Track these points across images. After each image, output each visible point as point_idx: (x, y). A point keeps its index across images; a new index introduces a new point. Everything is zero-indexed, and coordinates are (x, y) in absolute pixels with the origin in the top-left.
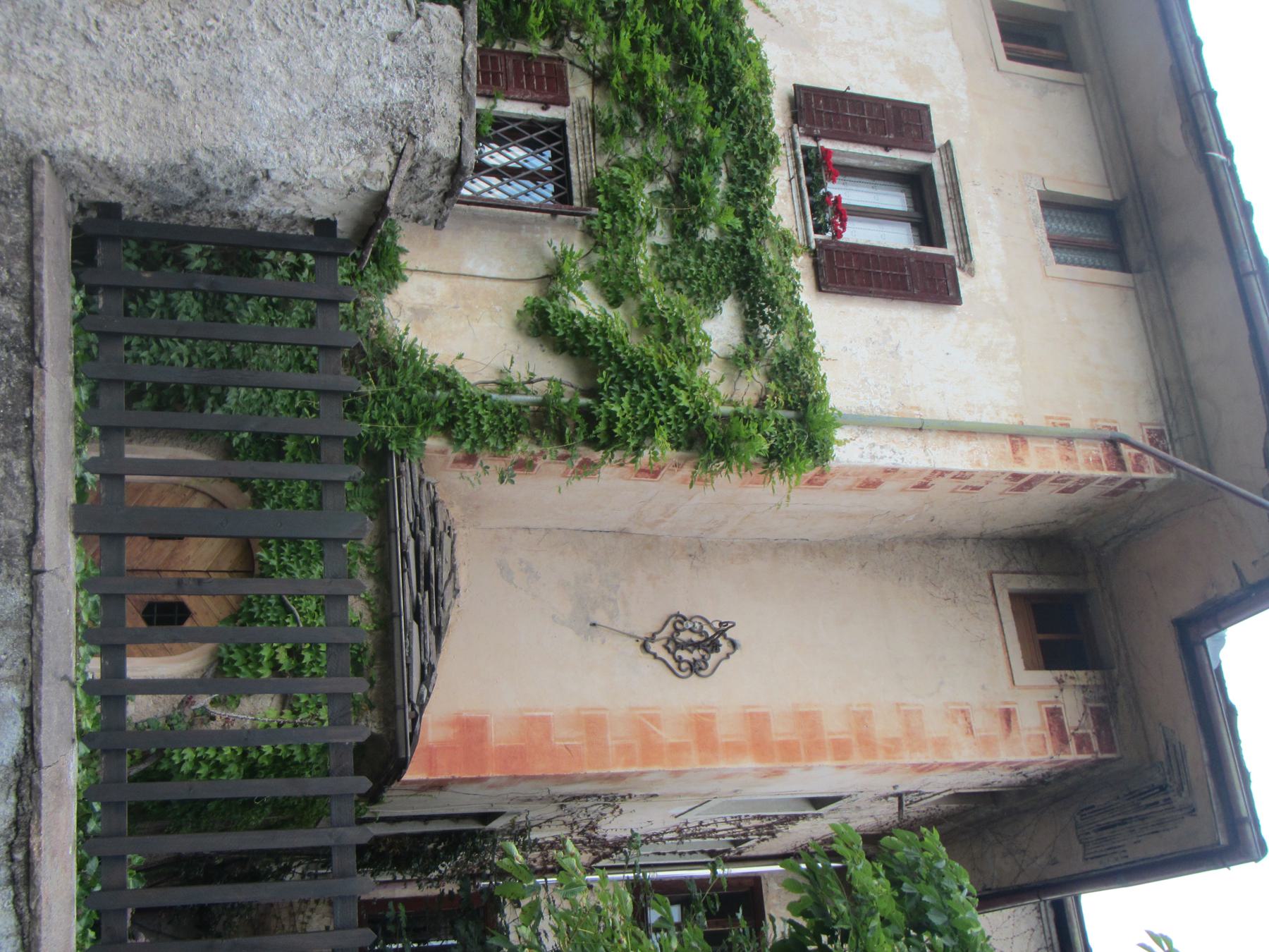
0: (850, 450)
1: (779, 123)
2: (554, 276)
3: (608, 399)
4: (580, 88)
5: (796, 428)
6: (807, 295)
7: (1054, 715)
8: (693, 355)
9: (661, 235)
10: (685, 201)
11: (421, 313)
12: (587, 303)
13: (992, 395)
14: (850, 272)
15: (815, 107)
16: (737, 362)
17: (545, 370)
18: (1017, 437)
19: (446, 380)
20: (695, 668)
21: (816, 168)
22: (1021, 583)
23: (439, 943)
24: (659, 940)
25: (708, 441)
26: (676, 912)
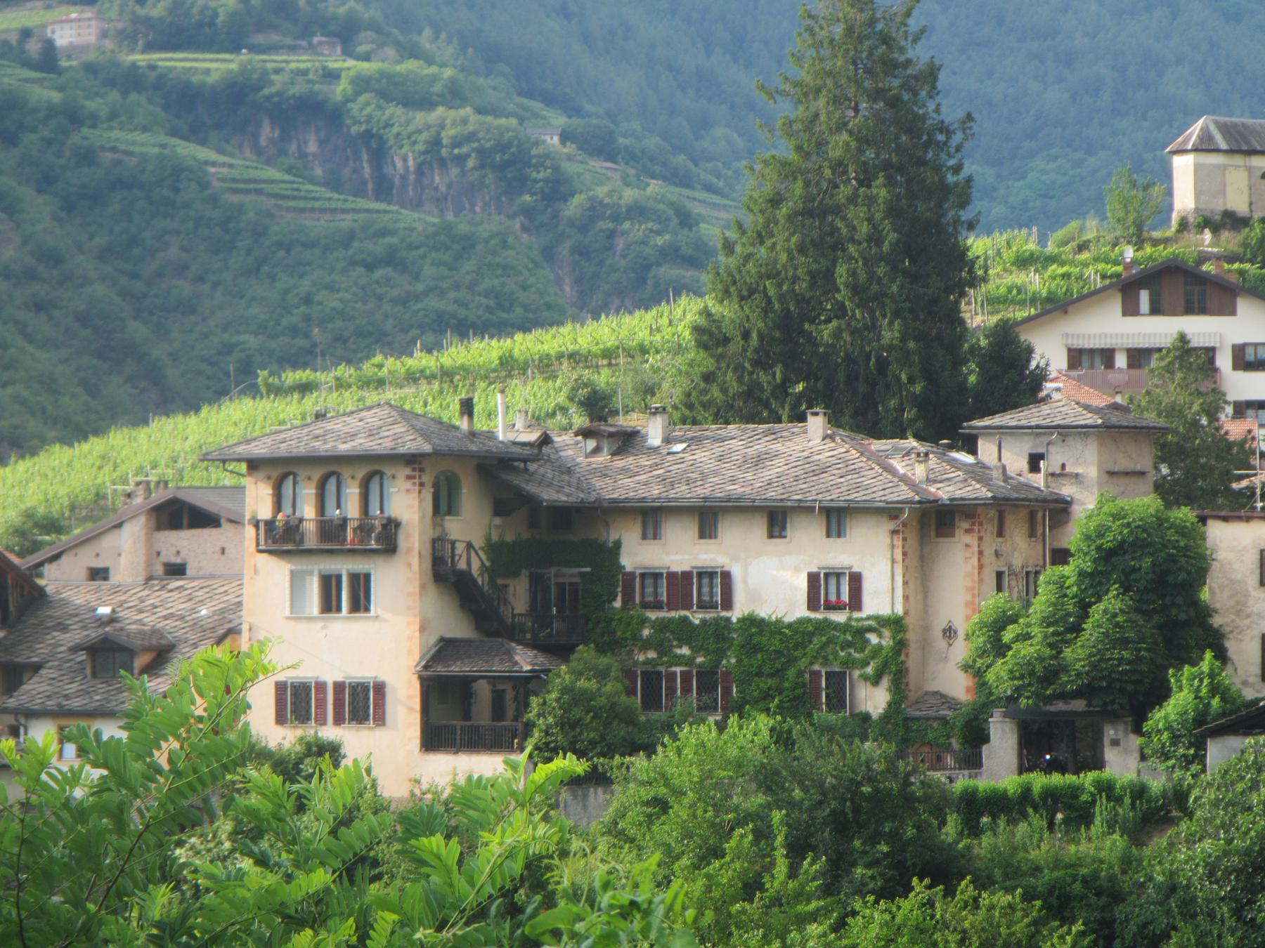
0: (899, 610)
1: (818, 616)
2: (865, 678)
3: (894, 668)
4: (816, 667)
5: (895, 624)
6: (863, 615)
7: (967, 531)
8: (880, 647)
9: (852, 651)
10: (847, 645)
11: (875, 708)
12: (869, 670)
13: (885, 565)
14: (856, 601)
15: (813, 604)
16: (880, 636)
17: (885, 682)
18: (893, 561)
19: (890, 704)
20: (955, 632)
21: (829, 607)
22: (933, 533)
23: (824, 685)
24: (401, 890)
25: (900, 646)
26: (696, 779)
